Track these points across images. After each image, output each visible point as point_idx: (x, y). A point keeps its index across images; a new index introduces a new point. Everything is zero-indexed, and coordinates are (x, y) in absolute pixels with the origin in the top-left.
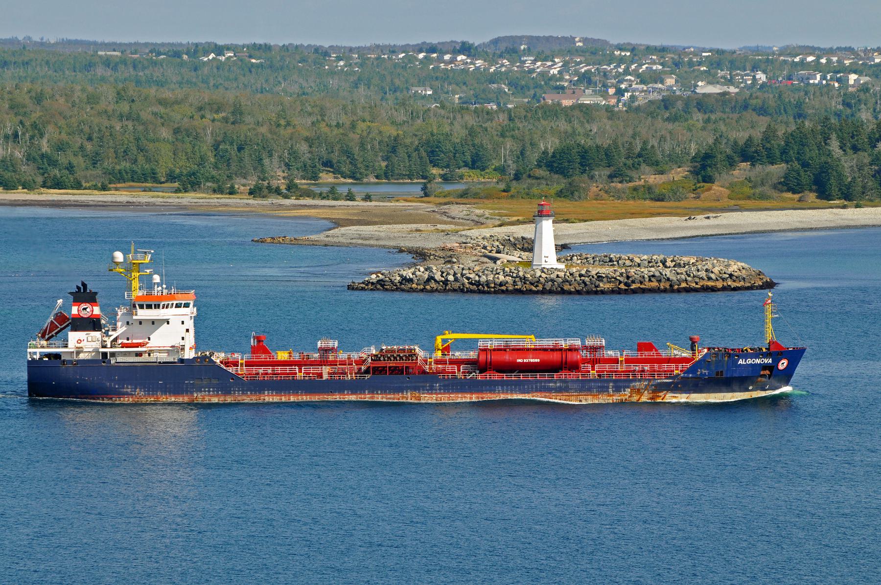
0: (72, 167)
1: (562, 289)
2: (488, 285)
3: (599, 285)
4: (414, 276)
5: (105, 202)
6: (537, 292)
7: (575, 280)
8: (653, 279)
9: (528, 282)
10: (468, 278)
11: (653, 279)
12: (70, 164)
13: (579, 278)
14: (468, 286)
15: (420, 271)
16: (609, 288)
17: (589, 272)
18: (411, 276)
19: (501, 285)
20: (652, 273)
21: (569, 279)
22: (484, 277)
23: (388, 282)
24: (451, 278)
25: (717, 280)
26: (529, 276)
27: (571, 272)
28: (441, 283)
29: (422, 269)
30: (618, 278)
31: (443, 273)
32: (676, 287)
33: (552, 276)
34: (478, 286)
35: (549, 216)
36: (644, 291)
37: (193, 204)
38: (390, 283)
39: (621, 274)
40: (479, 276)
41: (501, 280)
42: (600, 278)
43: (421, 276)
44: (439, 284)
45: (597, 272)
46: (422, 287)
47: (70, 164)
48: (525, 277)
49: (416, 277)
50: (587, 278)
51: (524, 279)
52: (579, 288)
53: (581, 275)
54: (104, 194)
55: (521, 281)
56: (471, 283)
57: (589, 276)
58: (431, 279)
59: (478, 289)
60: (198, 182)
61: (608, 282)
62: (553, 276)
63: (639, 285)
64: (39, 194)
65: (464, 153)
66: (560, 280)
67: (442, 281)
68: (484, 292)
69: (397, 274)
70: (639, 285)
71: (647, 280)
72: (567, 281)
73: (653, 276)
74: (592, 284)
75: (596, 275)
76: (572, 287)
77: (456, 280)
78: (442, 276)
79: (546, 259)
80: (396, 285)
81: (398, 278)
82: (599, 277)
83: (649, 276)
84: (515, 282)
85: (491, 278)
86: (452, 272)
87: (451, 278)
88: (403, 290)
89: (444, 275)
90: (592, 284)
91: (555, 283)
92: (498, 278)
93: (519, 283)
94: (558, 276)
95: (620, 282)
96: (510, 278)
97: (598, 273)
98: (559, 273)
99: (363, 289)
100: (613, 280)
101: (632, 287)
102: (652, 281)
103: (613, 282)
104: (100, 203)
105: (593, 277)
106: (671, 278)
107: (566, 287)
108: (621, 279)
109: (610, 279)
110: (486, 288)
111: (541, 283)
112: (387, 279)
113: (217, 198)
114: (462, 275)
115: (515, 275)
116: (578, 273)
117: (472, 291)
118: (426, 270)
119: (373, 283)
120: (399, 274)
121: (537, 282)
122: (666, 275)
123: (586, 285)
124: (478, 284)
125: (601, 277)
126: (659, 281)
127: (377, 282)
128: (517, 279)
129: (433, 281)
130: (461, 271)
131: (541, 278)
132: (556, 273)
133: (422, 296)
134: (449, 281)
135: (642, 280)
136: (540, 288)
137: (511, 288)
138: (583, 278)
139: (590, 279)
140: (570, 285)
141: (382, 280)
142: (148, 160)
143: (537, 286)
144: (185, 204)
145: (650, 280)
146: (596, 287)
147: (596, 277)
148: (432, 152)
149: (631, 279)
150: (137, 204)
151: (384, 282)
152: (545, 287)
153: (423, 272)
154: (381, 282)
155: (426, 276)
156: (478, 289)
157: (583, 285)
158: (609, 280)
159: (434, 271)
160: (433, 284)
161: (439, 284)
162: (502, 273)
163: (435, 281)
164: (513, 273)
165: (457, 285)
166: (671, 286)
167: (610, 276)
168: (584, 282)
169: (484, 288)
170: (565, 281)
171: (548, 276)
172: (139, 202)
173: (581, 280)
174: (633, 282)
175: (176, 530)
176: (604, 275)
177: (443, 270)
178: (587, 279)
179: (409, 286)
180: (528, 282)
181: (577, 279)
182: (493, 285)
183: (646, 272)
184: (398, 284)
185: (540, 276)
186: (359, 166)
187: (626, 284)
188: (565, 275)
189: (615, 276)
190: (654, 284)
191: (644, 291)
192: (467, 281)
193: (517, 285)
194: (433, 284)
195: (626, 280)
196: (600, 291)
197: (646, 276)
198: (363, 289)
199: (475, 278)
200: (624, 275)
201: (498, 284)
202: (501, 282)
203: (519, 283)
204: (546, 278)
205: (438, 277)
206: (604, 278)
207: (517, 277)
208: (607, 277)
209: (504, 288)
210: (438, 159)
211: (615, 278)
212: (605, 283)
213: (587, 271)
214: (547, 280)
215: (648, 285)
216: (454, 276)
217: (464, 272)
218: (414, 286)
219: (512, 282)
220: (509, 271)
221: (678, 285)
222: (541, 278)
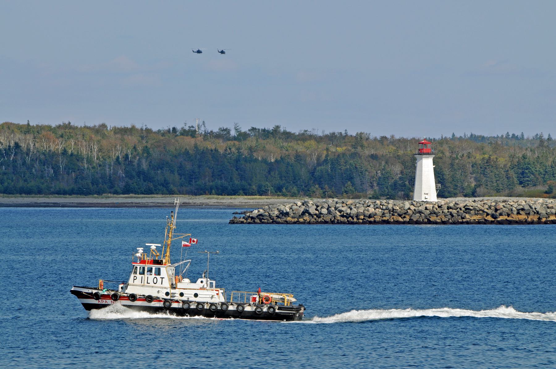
1: (428, 219)
2: (357, 216)
4: (291, 210)
5: (164, 203)
6: (404, 223)
7: (443, 212)
8: (521, 212)
9: (396, 214)
10: (340, 211)
11: (521, 212)
12: (165, 180)
13: (447, 211)
14: (339, 218)
15: (297, 205)
16: (475, 220)
17: (457, 204)
18: (288, 210)
19: (370, 216)
20: (521, 207)
21: (436, 211)
22: (355, 210)
23: (266, 216)
24: (324, 211)
26: (398, 208)
27: (440, 205)
28: (315, 216)
29: (299, 204)
30: (486, 210)
31: (317, 206)
32: (544, 220)
33: (420, 208)
34: (347, 218)
35: (428, 154)
36: (510, 222)
37: (243, 204)
38: (268, 218)
39: (490, 207)
40: (351, 209)
41: (370, 212)
42: (467, 210)
43: (297, 210)
44: (313, 217)
45: (465, 204)
46: (296, 220)
48: (393, 209)
49: (293, 211)
50: (454, 211)
51: (393, 211)
52: (444, 219)
53: (449, 208)
55: (390, 213)
56: (342, 216)
58: (306, 212)
59: (348, 221)
60: (266, 190)
61: (476, 214)
62: (422, 208)
63: (506, 217)
64: (106, 198)
65: (553, 174)
66: (428, 211)
67: (316, 214)
68: (352, 223)
69: (276, 209)
70: (506, 217)
71: (515, 213)
72: (435, 213)
74: (458, 216)
75: (464, 207)
76: (439, 218)
77: (329, 212)
78: (316, 210)
80: (273, 219)
81: (276, 213)
83: (518, 210)
84: (383, 214)
85: (361, 210)
86: (326, 206)
87: (324, 211)
88: (278, 223)
89: (319, 208)
90: (458, 216)
91: (422, 215)
92: (368, 211)
93: (387, 215)
94: (426, 209)
95: (488, 214)
96: (380, 210)
98: (428, 206)
99: (242, 222)
100: (481, 212)
101: (499, 219)
102: (521, 214)
103: (480, 214)
104: (159, 205)
105: (461, 209)
106: (540, 211)
107: (433, 218)
108: (489, 212)
109: (478, 212)
110: (355, 220)
111: (409, 215)
112: (267, 214)
113: (267, 199)
114: (336, 209)
115: (384, 207)
116: (447, 205)
117: (343, 223)
118: (303, 204)
119: (252, 218)
120: (278, 209)
121: (405, 214)
122: (535, 209)
123: (452, 216)
124: (348, 216)
127: (257, 216)
128: (386, 211)
129: (307, 214)
130: (335, 204)
131: (409, 211)
132: (425, 205)
133: (297, 226)
134: (322, 214)
135: (510, 212)
136: (407, 219)
137: (378, 219)
138: (451, 210)
139: (458, 212)
140: (437, 216)
141: (261, 215)
142: (242, 178)
143: (404, 217)
144: (237, 203)
145: (518, 213)
146: (463, 218)
147: (463, 209)
148: (523, 173)
149: (499, 212)
150: (192, 204)
151: (263, 216)
152: (412, 218)
153: (300, 207)
154: (260, 216)
155: (302, 209)
156: (348, 221)
157: (450, 217)
158: (476, 212)
159: (310, 205)
160: (307, 218)
161: (313, 217)
162: (372, 206)
164: (383, 205)
165: (328, 218)
166: (539, 219)
169: (353, 219)
170: (433, 213)
171: (416, 208)
172: (195, 203)
173: (448, 212)
174: (501, 214)
177: (318, 204)
178: (454, 212)
179: (285, 219)
180: (396, 214)
181: (444, 211)
182: (362, 217)
183: (516, 205)
184: (275, 218)
185: (409, 209)
186: (448, 185)
187: (493, 216)
188: (433, 207)
189: (483, 209)
190: (523, 217)
191: (510, 222)
192: (339, 214)
193: (385, 217)
194: (307, 218)
195: (494, 213)
196: (465, 222)
197: (514, 209)
198: (242, 222)
199: (346, 210)
200: (493, 208)
201: (368, 215)
202: (370, 214)
203: (387, 215)
204: (415, 210)
205: (312, 210)
206: (471, 210)
207: (386, 209)
208: (475, 209)
209: (372, 219)
210: (528, 181)
211: (483, 211)
212: (472, 215)
213: (455, 203)
214: (415, 212)
215: (515, 217)
216: (328, 209)
217: (337, 205)
218: (289, 219)
219: (381, 214)
220: (379, 204)
221: (546, 218)
222: (409, 211)
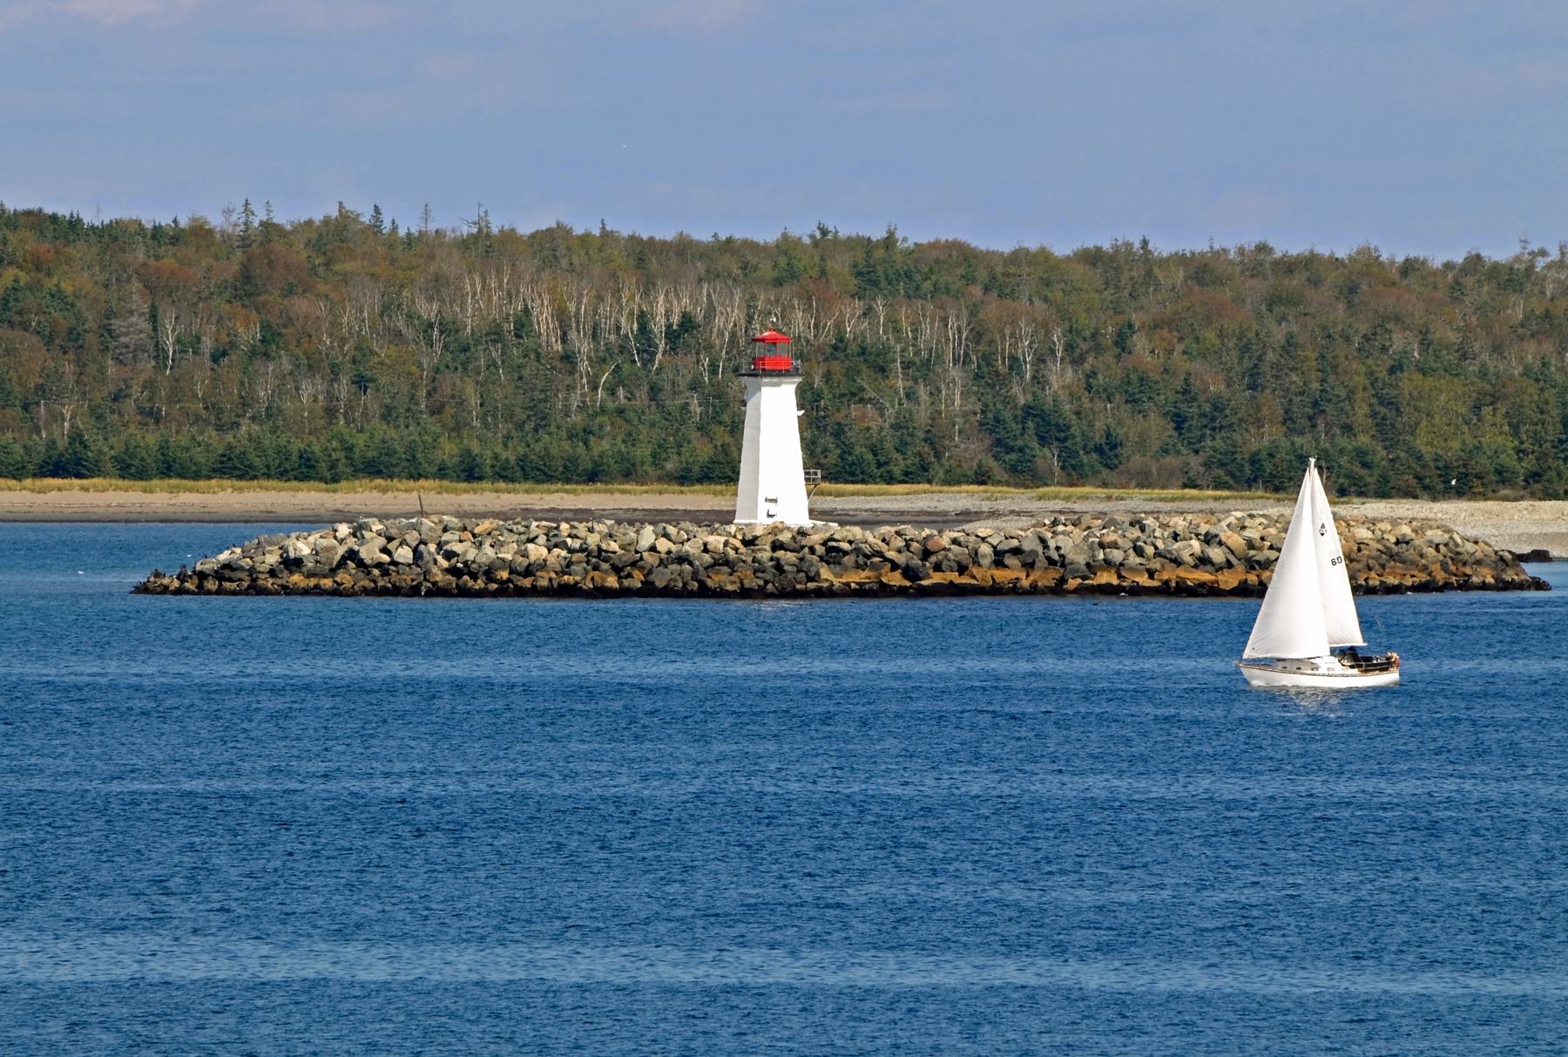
0: (1113, 447)
1: (702, 583)
3: (818, 574)
8: (1010, 560)
25: (1229, 565)
44: (369, 573)
47: (1108, 435)
54: (914, 493)
57: (803, 547)
73: (1017, 551)
75: (824, 543)
79: (771, 506)
82: (830, 550)
86: (412, 538)
97: (831, 539)
103: (874, 567)
105: (812, 550)
109: (866, 557)
113: (1216, 499)
116: (771, 538)
125: (837, 550)
126: (1029, 566)
147: (820, 550)
149: (933, 559)
152: (652, 577)
158: (861, 560)
163: (360, 564)
167: (867, 549)
168: (779, 567)
175: (593, 910)
176: (845, 546)
206: (846, 553)
208: (857, 551)
215: (985, 574)
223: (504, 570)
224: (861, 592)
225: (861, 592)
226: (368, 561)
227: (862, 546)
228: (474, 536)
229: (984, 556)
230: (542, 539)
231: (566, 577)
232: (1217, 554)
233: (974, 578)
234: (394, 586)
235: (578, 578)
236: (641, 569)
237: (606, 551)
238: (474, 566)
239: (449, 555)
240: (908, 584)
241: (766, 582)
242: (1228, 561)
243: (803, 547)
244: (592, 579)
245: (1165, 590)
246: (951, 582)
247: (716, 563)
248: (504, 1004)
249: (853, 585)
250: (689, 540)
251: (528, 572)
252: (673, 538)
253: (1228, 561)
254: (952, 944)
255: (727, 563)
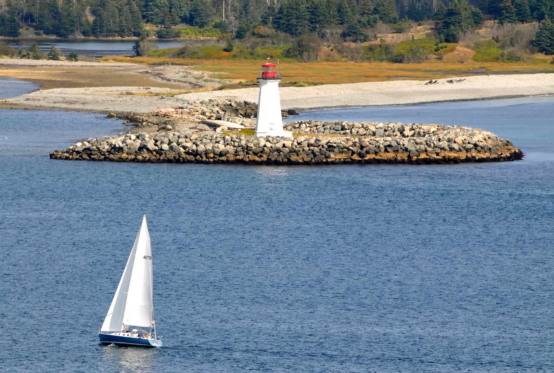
1: (289, 159)
8: (389, 149)
44: (152, 153)
57: (319, 145)
73: (390, 146)
82: (330, 146)
105: (323, 146)
109: (343, 149)
125: (332, 146)
147: (326, 146)
152: (270, 157)
158: (341, 150)
163: (148, 150)
176: (335, 145)
206: (335, 147)
215: (384, 156)
223: (212, 153)
224: (345, 163)
225: (345, 163)
226: (151, 149)
227: (340, 145)
228: (191, 140)
229: (382, 148)
230: (222, 142)
231: (238, 157)
232: (456, 146)
233: (381, 156)
234: (168, 159)
235: (243, 157)
236: (266, 153)
237: (250, 147)
238: (337, 161)
239: (184, 148)
240: (361, 159)
241: (312, 159)
242: (460, 149)
243: (319, 145)
244: (248, 157)
245: (468, 160)
246: (374, 158)
247: (290, 152)
248: (493, 333)
249: (342, 160)
250: (277, 143)
251: (221, 155)
252: (271, 142)
253: (460, 149)
254: (412, 286)
255: (295, 151)
